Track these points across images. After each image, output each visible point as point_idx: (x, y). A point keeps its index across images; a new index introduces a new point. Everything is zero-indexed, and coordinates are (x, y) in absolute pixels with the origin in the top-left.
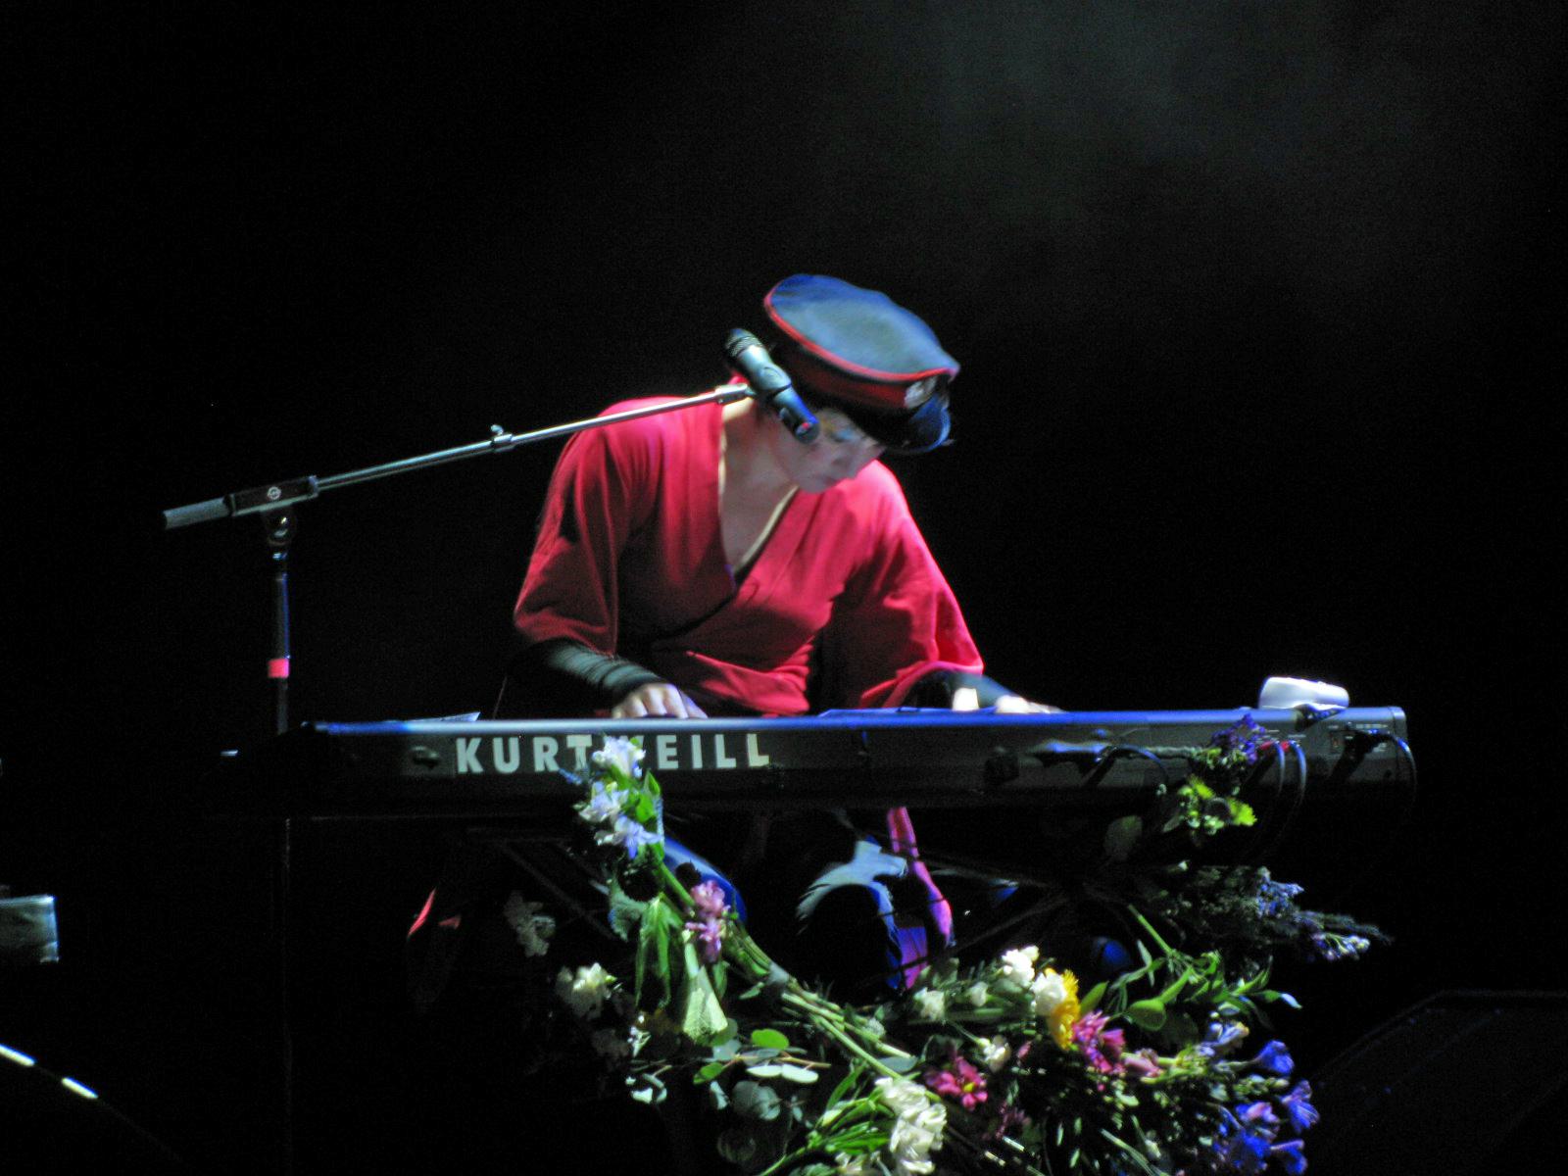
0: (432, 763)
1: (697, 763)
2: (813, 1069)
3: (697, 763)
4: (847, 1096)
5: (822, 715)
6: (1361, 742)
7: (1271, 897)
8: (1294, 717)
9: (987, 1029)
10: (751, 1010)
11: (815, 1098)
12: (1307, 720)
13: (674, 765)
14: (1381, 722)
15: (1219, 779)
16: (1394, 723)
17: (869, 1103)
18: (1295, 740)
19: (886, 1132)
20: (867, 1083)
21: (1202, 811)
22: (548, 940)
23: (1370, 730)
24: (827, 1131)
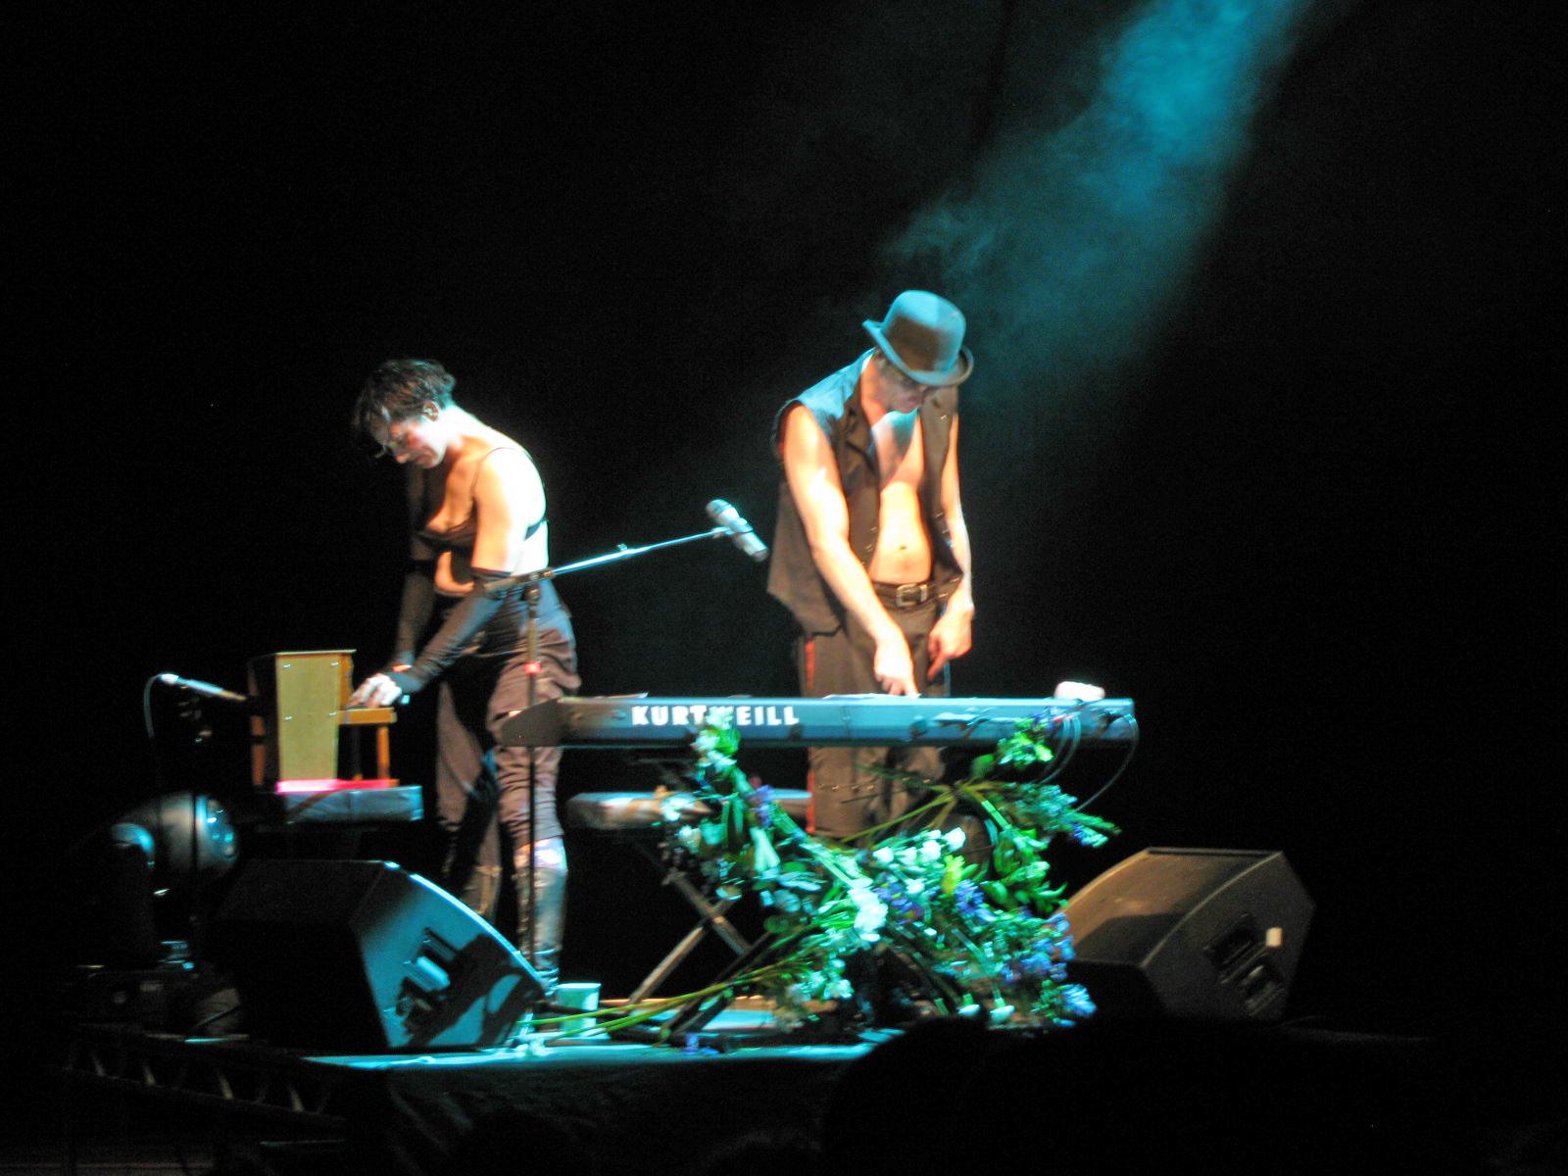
0: (621, 719)
1: (462, 1120)
2: (817, 884)
3: (462, 1120)
4: (833, 899)
5: (827, 697)
6: (1110, 718)
7: (1055, 802)
8: (1074, 703)
9: (913, 876)
10: (790, 853)
11: (818, 898)
12: (1081, 706)
13: (748, 722)
14: (1119, 707)
15: (1033, 735)
16: (1125, 707)
17: (845, 903)
18: (1074, 715)
19: (852, 918)
20: (843, 892)
21: (1017, 751)
22: (734, 757)
23: (1114, 712)
24: (824, 917)
